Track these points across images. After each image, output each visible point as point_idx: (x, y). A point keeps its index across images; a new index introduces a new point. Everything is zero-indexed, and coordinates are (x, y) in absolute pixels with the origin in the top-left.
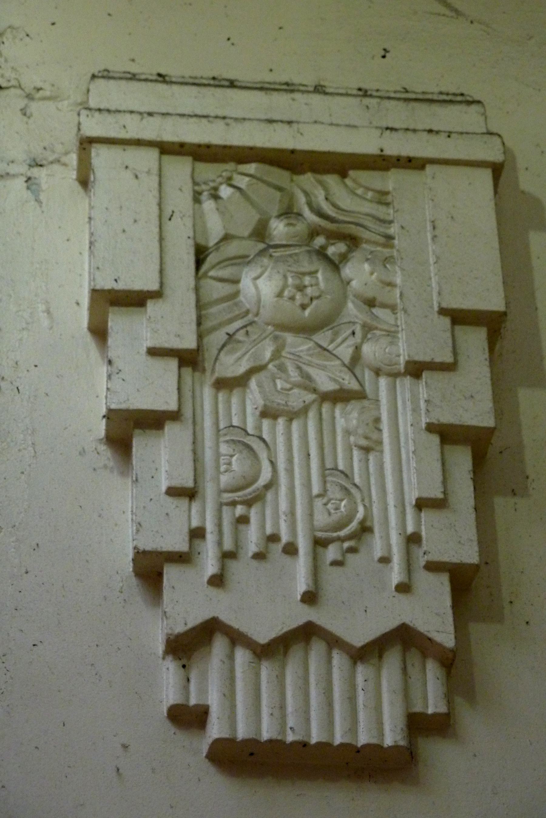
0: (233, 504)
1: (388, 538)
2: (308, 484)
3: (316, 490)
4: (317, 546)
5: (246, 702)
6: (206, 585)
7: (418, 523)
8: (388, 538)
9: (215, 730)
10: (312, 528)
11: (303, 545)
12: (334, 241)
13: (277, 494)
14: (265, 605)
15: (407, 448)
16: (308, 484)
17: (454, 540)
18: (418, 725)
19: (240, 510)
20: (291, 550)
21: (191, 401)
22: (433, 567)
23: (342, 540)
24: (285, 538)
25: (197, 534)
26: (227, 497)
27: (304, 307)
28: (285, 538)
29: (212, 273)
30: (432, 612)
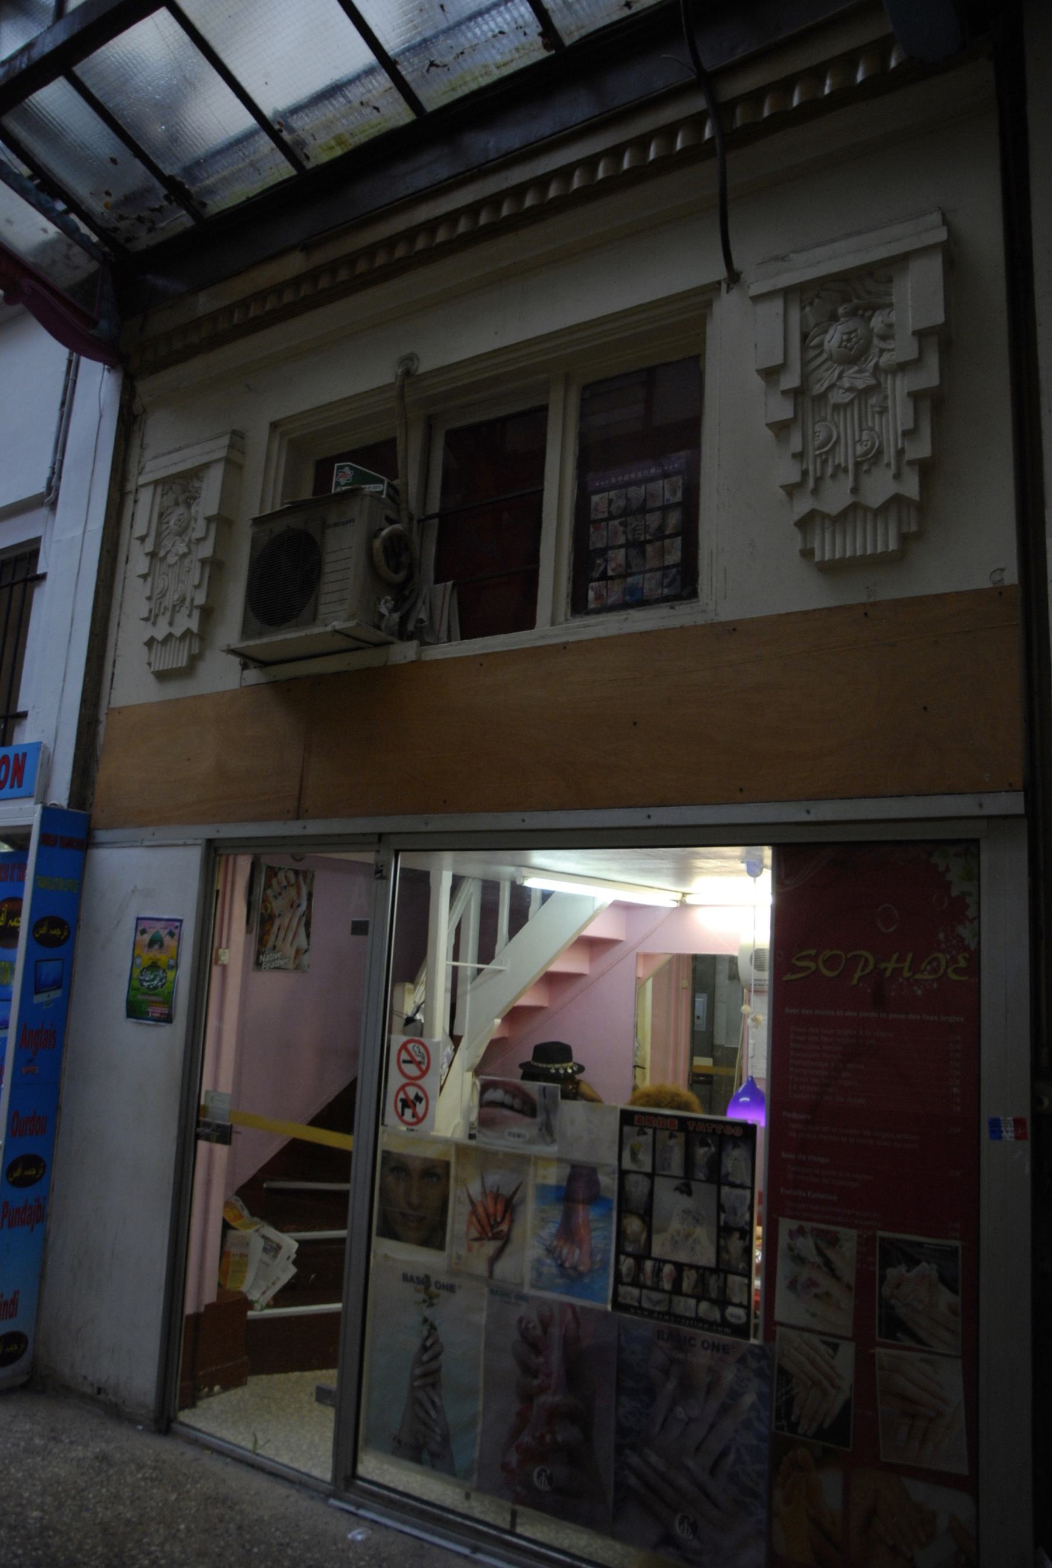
0: (821, 454)
1: (890, 455)
2: (854, 435)
3: (857, 438)
4: (567, 1171)
5: (829, 547)
6: (792, 523)
7: (903, 444)
8: (890, 455)
9: (817, 558)
10: (855, 457)
11: (851, 467)
12: (864, 311)
13: (815, 475)
14: (836, 497)
15: (898, 400)
16: (854, 435)
17: (922, 449)
18: (904, 538)
19: (824, 457)
20: (846, 470)
21: (555, 523)
22: (910, 463)
23: (870, 459)
24: (843, 465)
25: (805, 473)
26: (818, 452)
27: (851, 350)
28: (843, 465)
29: (812, 344)
30: (911, 488)
